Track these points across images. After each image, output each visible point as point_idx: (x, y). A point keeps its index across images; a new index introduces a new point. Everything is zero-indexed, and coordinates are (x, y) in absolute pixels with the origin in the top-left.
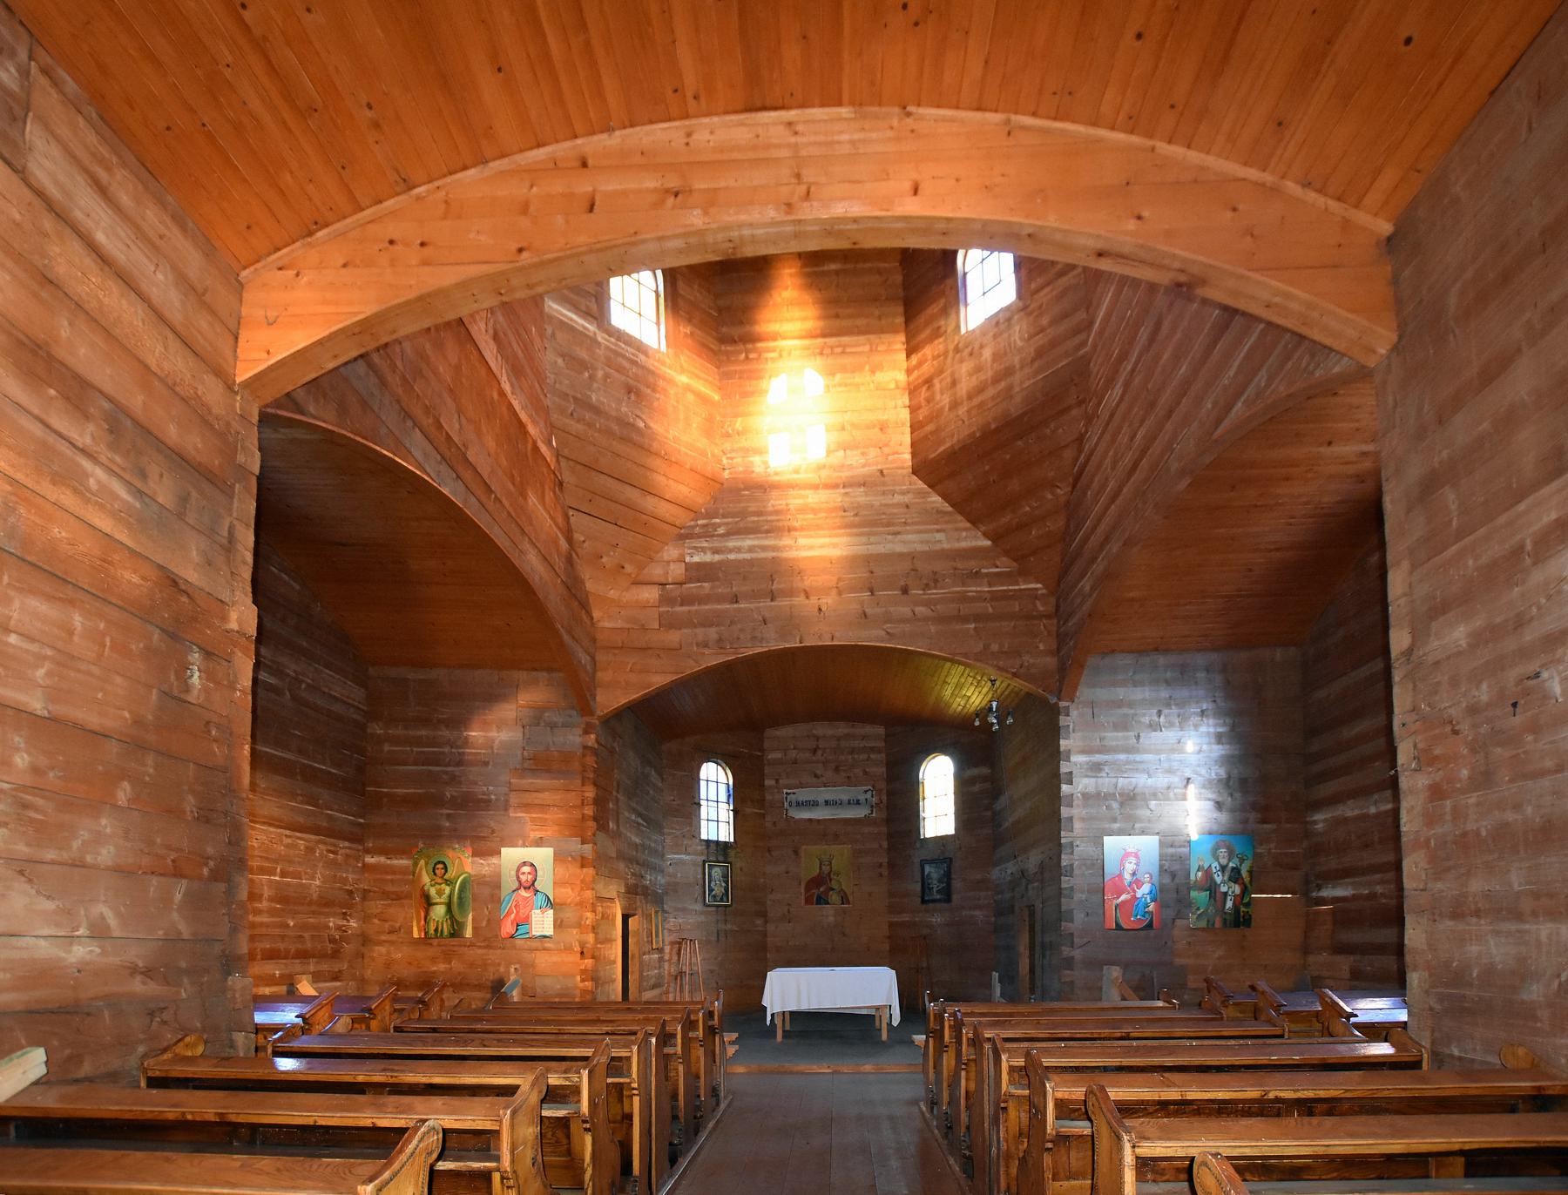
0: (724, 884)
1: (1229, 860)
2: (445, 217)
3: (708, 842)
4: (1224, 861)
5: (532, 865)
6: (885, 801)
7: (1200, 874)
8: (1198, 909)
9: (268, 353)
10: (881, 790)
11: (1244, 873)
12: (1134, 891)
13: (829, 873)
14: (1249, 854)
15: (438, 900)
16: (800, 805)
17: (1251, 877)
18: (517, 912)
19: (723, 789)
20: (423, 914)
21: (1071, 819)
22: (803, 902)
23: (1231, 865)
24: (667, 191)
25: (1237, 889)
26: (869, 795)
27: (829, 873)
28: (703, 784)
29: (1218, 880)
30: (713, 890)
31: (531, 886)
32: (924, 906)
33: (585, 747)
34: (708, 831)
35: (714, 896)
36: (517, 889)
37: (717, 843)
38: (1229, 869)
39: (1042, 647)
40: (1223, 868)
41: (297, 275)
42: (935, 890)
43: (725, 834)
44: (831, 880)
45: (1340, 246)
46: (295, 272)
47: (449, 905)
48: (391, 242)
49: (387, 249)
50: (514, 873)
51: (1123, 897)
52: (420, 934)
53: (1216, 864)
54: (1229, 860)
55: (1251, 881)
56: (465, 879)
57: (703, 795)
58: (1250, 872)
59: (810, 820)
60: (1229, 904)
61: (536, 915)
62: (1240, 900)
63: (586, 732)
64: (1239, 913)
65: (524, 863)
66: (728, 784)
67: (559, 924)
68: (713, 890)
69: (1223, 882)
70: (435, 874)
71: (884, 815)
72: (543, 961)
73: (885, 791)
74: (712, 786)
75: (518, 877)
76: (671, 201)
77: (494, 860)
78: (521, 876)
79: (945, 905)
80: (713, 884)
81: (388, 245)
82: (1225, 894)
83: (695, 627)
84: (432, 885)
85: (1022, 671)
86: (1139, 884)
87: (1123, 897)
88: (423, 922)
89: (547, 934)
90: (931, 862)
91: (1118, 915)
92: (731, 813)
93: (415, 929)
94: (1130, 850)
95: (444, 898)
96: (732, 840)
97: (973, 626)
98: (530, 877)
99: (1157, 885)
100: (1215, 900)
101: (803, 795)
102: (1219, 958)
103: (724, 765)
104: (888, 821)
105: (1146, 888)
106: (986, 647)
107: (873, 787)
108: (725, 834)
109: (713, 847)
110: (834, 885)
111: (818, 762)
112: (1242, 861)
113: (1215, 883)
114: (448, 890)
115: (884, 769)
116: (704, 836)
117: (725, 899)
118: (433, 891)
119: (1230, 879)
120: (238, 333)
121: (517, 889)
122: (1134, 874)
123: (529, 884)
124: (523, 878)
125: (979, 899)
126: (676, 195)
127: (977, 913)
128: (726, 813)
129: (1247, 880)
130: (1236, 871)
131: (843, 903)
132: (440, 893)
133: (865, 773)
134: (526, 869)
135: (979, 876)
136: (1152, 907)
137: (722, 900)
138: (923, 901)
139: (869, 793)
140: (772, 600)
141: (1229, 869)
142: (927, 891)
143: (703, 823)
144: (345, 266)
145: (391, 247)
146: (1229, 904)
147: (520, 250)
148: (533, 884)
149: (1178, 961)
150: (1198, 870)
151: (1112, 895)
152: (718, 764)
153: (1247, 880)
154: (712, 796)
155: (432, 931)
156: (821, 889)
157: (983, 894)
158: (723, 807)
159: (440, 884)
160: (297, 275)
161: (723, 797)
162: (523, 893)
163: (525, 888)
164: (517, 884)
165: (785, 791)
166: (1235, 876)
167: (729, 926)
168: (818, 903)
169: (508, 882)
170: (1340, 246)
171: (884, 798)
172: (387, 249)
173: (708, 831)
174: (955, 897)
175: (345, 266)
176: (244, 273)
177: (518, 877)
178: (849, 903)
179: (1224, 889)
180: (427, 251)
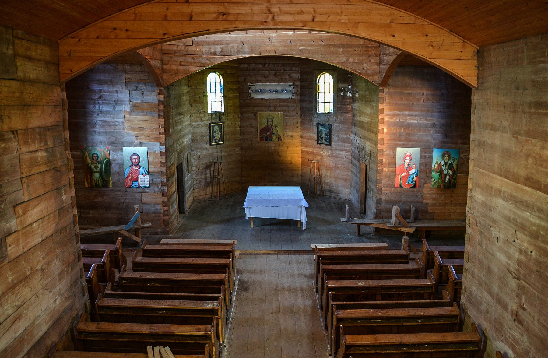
0: (220, 133)
1: (449, 160)
2: (135, 20)
3: (212, 114)
4: (446, 161)
5: (137, 155)
6: (299, 91)
7: (436, 165)
8: (435, 180)
9: (71, 71)
10: (297, 86)
11: (454, 166)
12: (409, 172)
13: (272, 126)
14: (457, 157)
15: (96, 171)
16: (256, 91)
17: (457, 167)
18: (132, 177)
19: (218, 85)
20: (89, 177)
21: (383, 139)
22: (259, 139)
23: (449, 162)
24: (220, 13)
25: (451, 173)
26: (292, 87)
27: (272, 126)
28: (208, 84)
29: (444, 168)
30: (215, 137)
31: (138, 165)
32: (318, 145)
33: (159, 101)
34: (211, 108)
35: (215, 140)
36: (131, 166)
37: (216, 113)
38: (448, 164)
39: (373, 61)
40: (446, 163)
41: (79, 40)
42: (323, 139)
43: (220, 108)
44: (272, 129)
45: (461, 52)
46: (78, 39)
47: (101, 173)
48: (115, 29)
49: (113, 31)
50: (129, 158)
51: (404, 174)
52: (88, 185)
53: (443, 162)
54: (449, 160)
55: (457, 170)
56: (107, 161)
57: (208, 90)
58: (457, 165)
59: (262, 99)
60: (447, 179)
61: (141, 177)
62: (451, 177)
63: (159, 94)
64: (451, 182)
65: (134, 154)
66: (221, 83)
67: (152, 183)
68: (215, 137)
69: (446, 169)
70: (93, 159)
71: (298, 98)
72: (147, 198)
73: (299, 86)
74: (213, 84)
75: (131, 161)
76: (221, 18)
77: (119, 153)
78: (133, 160)
79: (329, 147)
80: (214, 134)
81: (113, 30)
82: (446, 174)
83: (210, 45)
84: (92, 164)
85: (364, 72)
86: (411, 169)
87: (404, 174)
88: (89, 180)
89: (147, 186)
90: (322, 125)
91: (401, 182)
92: (223, 98)
93: (86, 183)
94: (408, 154)
95: (98, 170)
96: (223, 111)
97: (341, 50)
98: (137, 160)
99: (418, 169)
100: (442, 177)
101: (259, 86)
102: (442, 200)
103: (219, 74)
104: (301, 101)
105: (413, 171)
106: (347, 60)
107: (294, 84)
108: (220, 108)
109: (214, 116)
110: (274, 132)
111: (266, 70)
112: (454, 160)
113: (442, 169)
114: (99, 166)
115: (299, 75)
116: (209, 111)
117: (220, 141)
118: (93, 166)
119: (448, 168)
120: (59, 63)
121: (131, 166)
122: (409, 164)
123: (137, 164)
124: (134, 161)
125: (345, 147)
126: (223, 15)
127: (344, 153)
128: (220, 98)
129: (455, 168)
130: (451, 165)
131: (278, 141)
132: (96, 167)
133: (290, 76)
134: (135, 157)
135: (345, 136)
136: (415, 179)
137: (219, 141)
138: (318, 143)
139: (292, 87)
140: (246, 34)
141: (448, 164)
142: (320, 138)
143: (209, 104)
144: (97, 38)
145: (115, 31)
146: (447, 179)
147: (164, 34)
148: (139, 164)
149: (425, 201)
150: (436, 164)
151: (399, 173)
152: (215, 73)
153: (455, 168)
154: (213, 90)
155: (94, 185)
156: (268, 134)
157: (346, 144)
158: (219, 94)
159: (96, 163)
160: (79, 40)
161: (218, 89)
162: (134, 167)
163: (135, 165)
164: (131, 163)
165: (249, 84)
166: (451, 167)
167: (223, 153)
168: (266, 140)
169: (128, 163)
170: (461, 52)
171: (299, 89)
172: (113, 31)
173: (211, 108)
174: (333, 143)
175: (97, 38)
176: (59, 41)
177: (131, 161)
178: (282, 141)
179: (445, 172)
180: (129, 33)
